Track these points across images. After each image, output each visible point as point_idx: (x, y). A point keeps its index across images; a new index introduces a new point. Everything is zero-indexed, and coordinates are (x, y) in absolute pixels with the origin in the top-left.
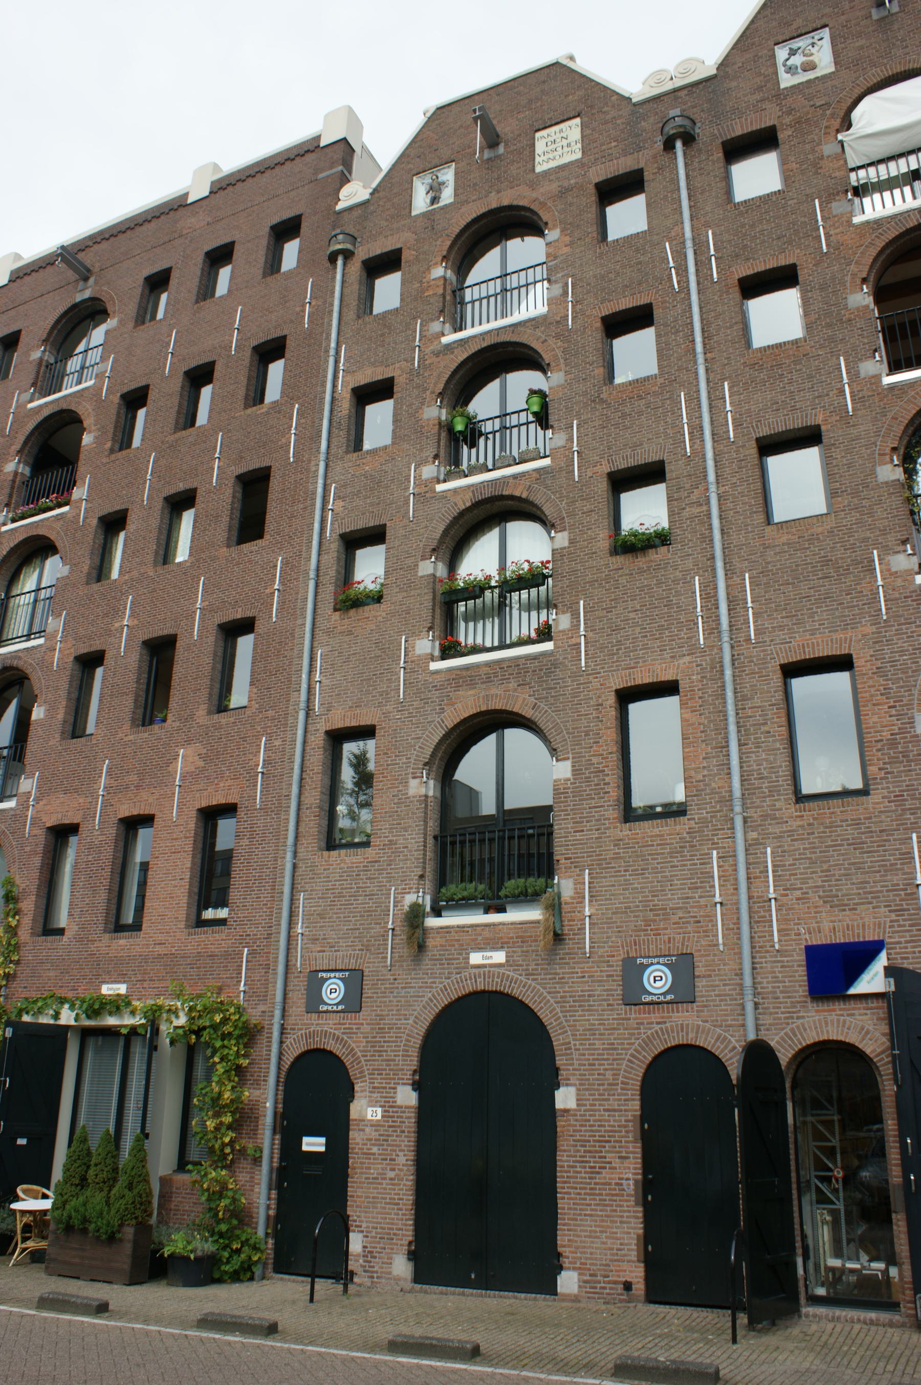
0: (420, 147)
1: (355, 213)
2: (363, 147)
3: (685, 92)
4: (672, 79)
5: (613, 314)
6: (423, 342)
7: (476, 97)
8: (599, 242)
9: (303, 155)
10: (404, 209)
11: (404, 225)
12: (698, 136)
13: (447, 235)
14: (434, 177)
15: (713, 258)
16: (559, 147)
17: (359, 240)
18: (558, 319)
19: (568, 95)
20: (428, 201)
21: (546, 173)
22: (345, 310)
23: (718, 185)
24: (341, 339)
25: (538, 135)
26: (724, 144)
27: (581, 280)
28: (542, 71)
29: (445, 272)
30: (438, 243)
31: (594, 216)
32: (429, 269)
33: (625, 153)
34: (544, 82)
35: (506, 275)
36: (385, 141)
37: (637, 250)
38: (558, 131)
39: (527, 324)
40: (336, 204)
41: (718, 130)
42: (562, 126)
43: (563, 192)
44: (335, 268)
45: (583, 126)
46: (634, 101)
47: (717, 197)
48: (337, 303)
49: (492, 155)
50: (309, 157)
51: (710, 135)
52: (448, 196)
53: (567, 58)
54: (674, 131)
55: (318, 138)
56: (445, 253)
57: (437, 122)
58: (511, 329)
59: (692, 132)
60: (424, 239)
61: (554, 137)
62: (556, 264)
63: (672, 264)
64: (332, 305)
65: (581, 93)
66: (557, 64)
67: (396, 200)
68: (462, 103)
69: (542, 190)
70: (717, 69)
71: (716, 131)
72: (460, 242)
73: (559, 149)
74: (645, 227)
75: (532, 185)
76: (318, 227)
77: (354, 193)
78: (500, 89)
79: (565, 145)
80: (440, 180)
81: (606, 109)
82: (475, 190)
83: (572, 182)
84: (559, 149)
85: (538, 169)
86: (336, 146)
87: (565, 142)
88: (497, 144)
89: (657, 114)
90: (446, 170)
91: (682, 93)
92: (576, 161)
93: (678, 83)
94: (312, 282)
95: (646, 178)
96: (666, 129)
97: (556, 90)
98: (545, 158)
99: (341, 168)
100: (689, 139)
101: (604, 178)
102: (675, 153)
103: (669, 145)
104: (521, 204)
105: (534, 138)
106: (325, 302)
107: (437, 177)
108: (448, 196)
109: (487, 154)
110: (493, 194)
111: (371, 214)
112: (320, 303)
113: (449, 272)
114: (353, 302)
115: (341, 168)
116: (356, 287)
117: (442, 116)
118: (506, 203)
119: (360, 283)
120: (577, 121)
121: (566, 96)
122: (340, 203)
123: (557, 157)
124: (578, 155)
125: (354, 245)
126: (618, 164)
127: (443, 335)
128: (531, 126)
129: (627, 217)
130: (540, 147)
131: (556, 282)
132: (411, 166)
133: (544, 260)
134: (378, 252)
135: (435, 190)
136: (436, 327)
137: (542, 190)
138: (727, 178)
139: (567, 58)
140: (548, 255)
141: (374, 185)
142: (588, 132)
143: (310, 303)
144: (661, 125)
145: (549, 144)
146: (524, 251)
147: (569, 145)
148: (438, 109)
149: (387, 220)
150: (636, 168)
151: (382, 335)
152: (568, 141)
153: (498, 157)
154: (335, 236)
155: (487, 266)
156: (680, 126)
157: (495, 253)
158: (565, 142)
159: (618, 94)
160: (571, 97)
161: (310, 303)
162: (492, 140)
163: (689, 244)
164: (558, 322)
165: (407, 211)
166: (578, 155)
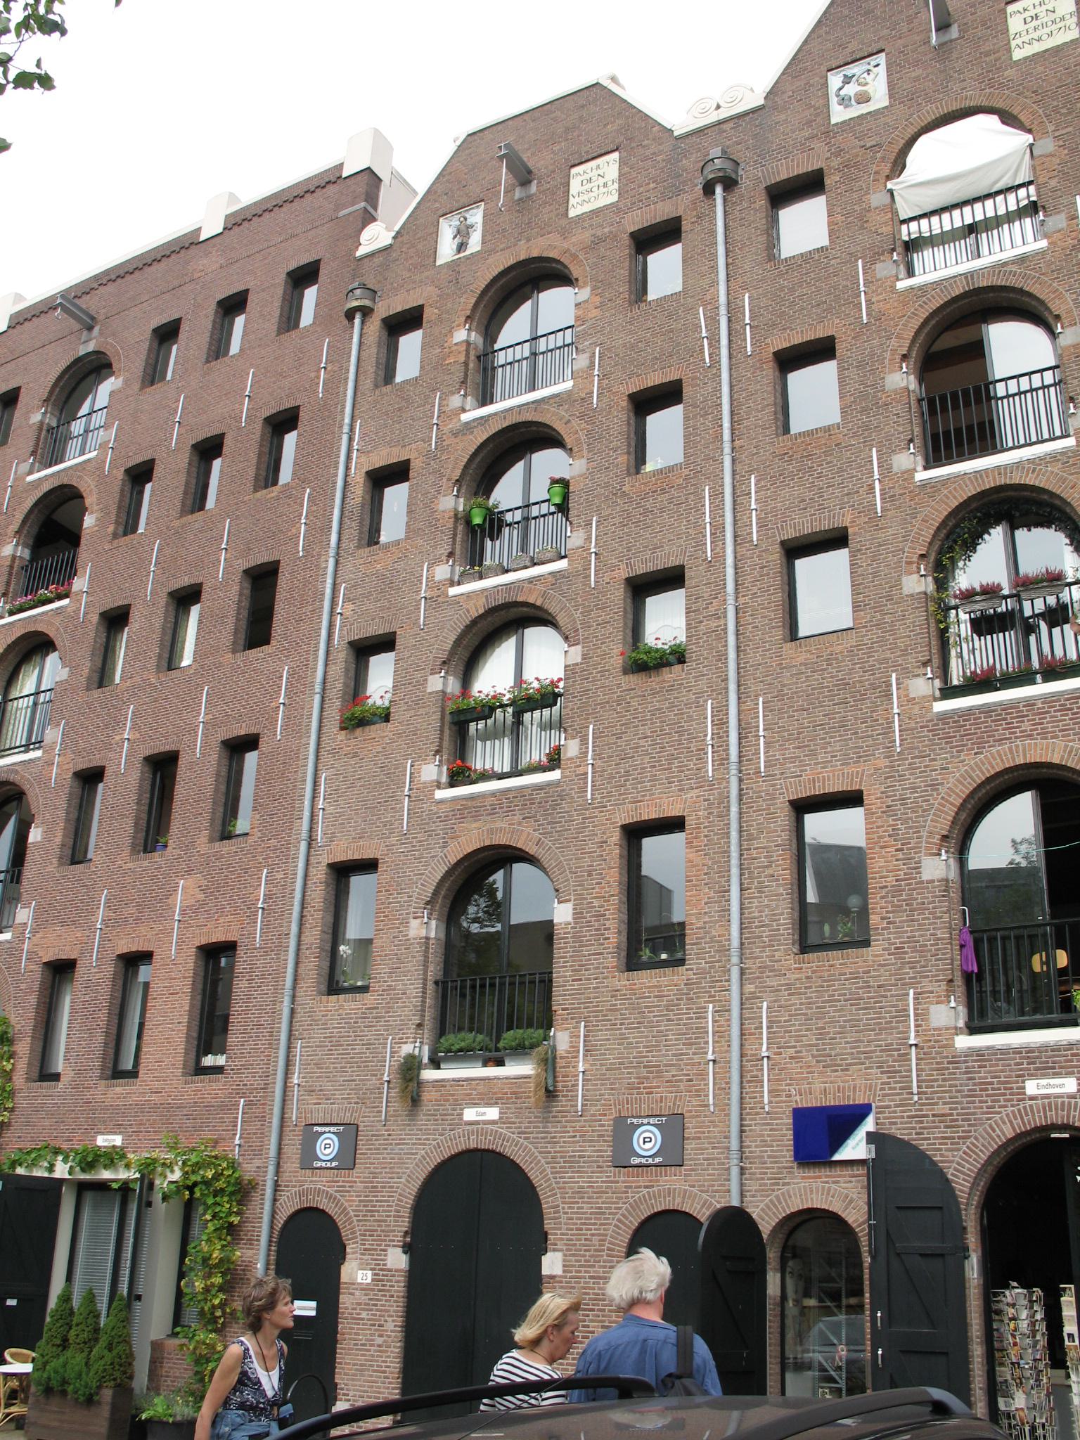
50: (331, 189)
87: (601, 181)
149: (410, 270)
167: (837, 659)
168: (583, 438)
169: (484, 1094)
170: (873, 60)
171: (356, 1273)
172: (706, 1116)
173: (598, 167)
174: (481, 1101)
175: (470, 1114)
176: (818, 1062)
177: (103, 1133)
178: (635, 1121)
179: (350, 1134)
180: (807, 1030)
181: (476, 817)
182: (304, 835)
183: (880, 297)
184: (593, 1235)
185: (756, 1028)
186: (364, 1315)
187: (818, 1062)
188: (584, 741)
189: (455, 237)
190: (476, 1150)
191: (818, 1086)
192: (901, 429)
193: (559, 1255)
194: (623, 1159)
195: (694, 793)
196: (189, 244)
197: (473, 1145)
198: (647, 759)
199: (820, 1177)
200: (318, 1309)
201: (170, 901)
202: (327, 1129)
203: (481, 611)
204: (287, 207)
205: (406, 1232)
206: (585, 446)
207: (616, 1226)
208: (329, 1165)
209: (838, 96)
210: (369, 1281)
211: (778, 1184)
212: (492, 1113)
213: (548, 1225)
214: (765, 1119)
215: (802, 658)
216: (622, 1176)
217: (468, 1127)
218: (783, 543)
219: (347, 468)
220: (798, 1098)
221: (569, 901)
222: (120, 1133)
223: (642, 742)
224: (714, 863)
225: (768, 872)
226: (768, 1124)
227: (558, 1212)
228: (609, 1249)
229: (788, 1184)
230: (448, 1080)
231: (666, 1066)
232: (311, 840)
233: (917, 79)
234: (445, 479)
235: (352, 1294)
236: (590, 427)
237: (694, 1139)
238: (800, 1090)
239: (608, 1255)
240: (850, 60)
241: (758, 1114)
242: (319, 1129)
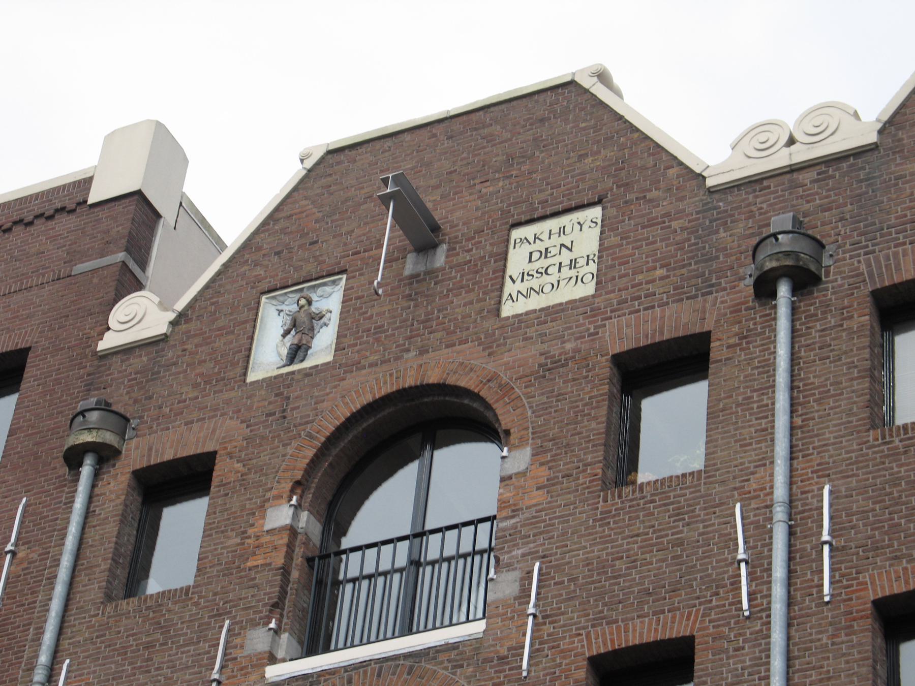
0: (284, 231)
1: (139, 361)
2: (185, 207)
3: (812, 174)
4: (791, 141)
5: (615, 652)
6: (227, 671)
7: (407, 137)
8: (605, 487)
9: (50, 218)
10: (234, 364)
11: (228, 402)
12: (827, 274)
13: (310, 435)
14: (303, 302)
15: (826, 548)
16: (553, 265)
17: (134, 423)
18: (504, 651)
19: (586, 155)
20: (285, 352)
21: (520, 319)
22: (82, 578)
23: (856, 385)
24: (65, 644)
25: (516, 234)
26: (875, 294)
27: (558, 568)
28: (542, 97)
29: (295, 516)
30: (290, 450)
31: (602, 427)
32: (262, 508)
33: (680, 295)
34: (542, 120)
35: (415, 536)
36: (233, 192)
37: (678, 514)
38: (555, 230)
39: (442, 657)
40: (101, 336)
41: (869, 265)
42: (565, 220)
43: (551, 366)
44: (76, 480)
45: (607, 227)
46: (710, 183)
47: (850, 413)
48: (66, 561)
49: (421, 268)
50: (64, 223)
51: (851, 276)
52: (323, 347)
53: (592, 75)
54: (774, 264)
55: (85, 183)
56: (299, 475)
57: (324, 181)
58: (408, 663)
59: (813, 268)
60: (263, 438)
61: (547, 243)
62: (514, 527)
63: (741, 555)
64: (57, 563)
65: (609, 153)
66: (571, 84)
67: (219, 344)
68: (378, 145)
69: (507, 358)
70: (880, 132)
71: (863, 267)
72: (335, 451)
73: (553, 270)
74: (698, 464)
75: (491, 345)
76: (57, 382)
77: (139, 318)
78: (457, 126)
79: (566, 262)
80: (313, 308)
81: (654, 194)
82: (378, 340)
83: (569, 346)
84: (553, 270)
85: (508, 310)
86: (119, 207)
87: (566, 257)
88: (435, 246)
89: (751, 215)
90: (328, 289)
91: (806, 177)
92: (582, 300)
93: (800, 154)
94: (26, 506)
95: (713, 355)
96: (760, 256)
97: (563, 140)
98: (523, 287)
99: (121, 256)
100: (805, 280)
101: (633, 345)
102: (775, 307)
103: (764, 289)
104: (462, 383)
105: (508, 241)
106: (44, 555)
107: (310, 302)
108: (323, 347)
109: (411, 265)
110: (412, 354)
111: (168, 366)
112: (35, 556)
113: (304, 516)
114: (101, 561)
115: (121, 256)
116: (112, 528)
117: (335, 170)
118: (433, 378)
119: (123, 520)
120: (596, 212)
121: (581, 157)
122: (107, 335)
123: (547, 288)
124: (588, 289)
125: (122, 435)
126: (663, 317)
127: (273, 659)
128: (505, 213)
129: (675, 428)
130: (517, 261)
131: (509, 567)
132: (260, 271)
133: (492, 511)
134: (169, 456)
135: (302, 329)
136: (258, 640)
137: (507, 358)
138: (882, 361)
139: (592, 75)
140: (503, 504)
141: (180, 305)
142: (614, 240)
143: (14, 553)
144: (758, 239)
145: (536, 256)
146: (465, 478)
147: (573, 264)
148: (330, 152)
149: (196, 386)
150: (697, 330)
151: (149, 646)
152: (572, 256)
153: (431, 273)
154: (82, 413)
155: (385, 510)
156: (787, 254)
157: (406, 477)
158: (566, 257)
159: (681, 164)
160: (590, 159)
161: (14, 553)
162: (423, 234)
163: (780, 513)
164: (501, 658)
165: (239, 370)
166: (588, 289)
173: (562, 231)
189: (286, 334)
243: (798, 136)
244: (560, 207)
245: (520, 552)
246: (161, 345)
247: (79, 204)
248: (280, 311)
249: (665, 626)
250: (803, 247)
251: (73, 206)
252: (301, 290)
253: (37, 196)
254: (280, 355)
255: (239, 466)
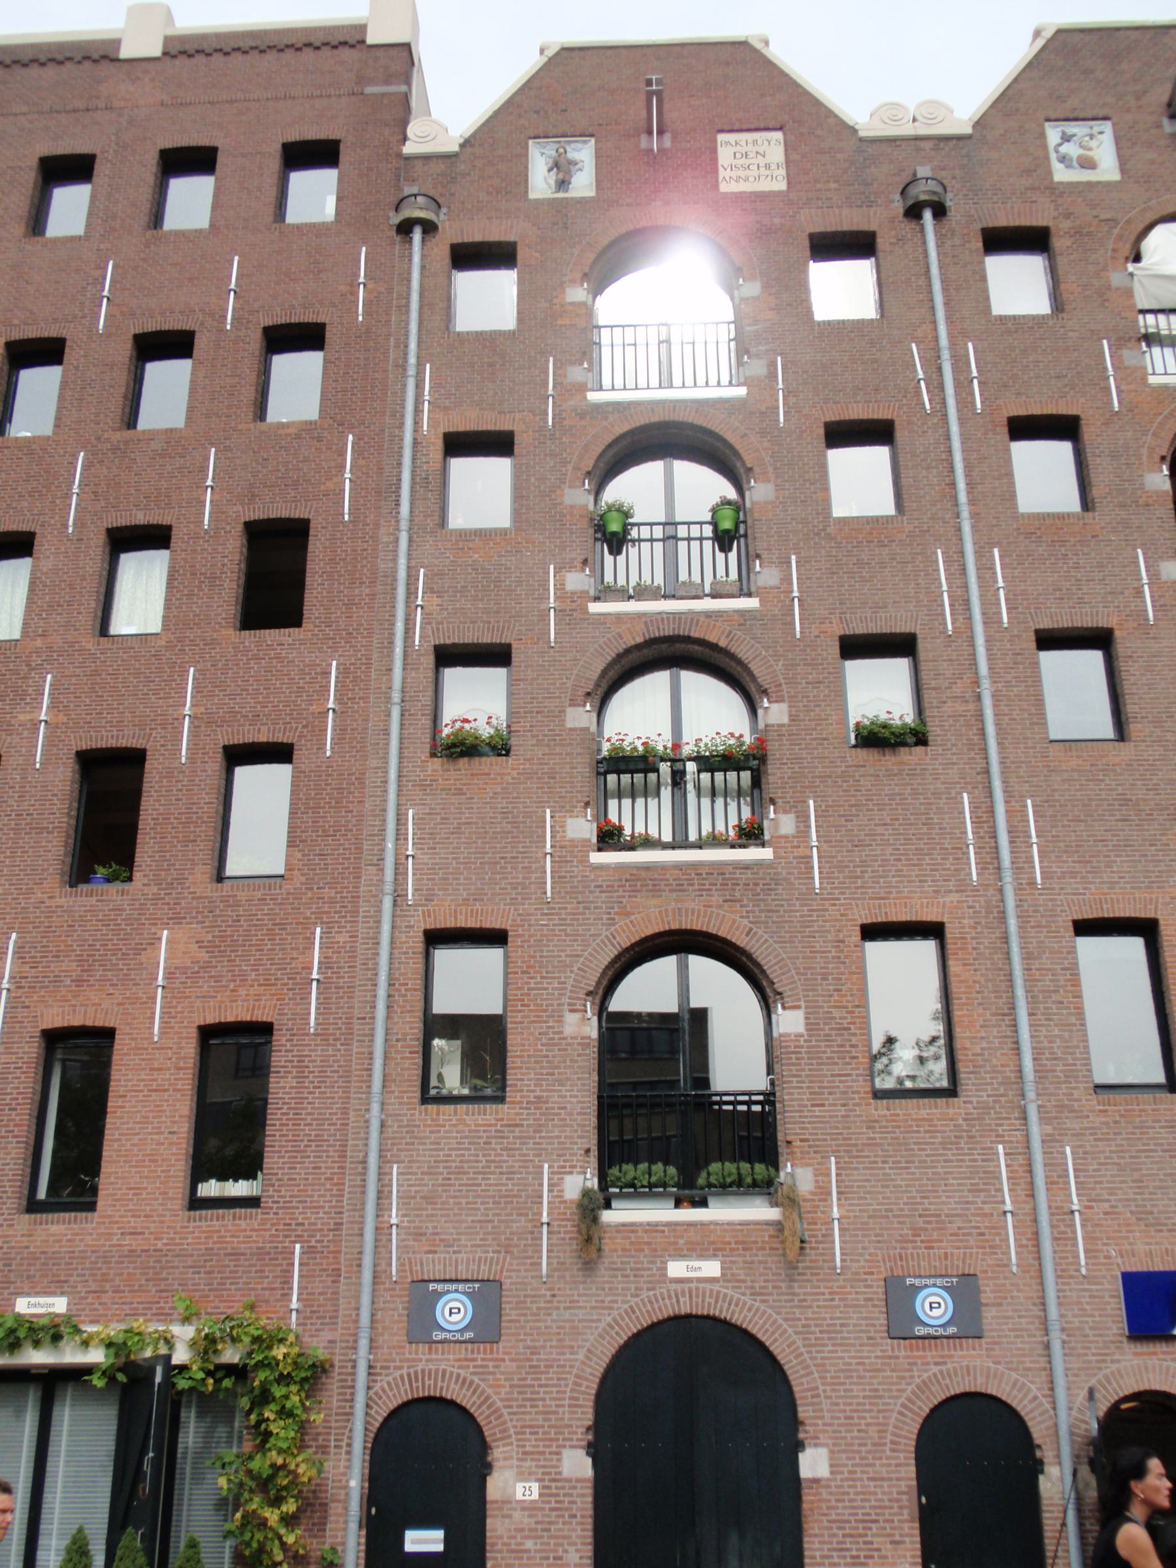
50: (345, 54)
83: (777, 221)
87: (761, 161)
90: (579, 145)
93: (923, 131)
98: (734, 174)
100: (940, 211)
121: (762, 96)
145: (738, 156)
149: (489, 193)
151: (491, 365)
167: (1114, 771)
168: (767, 459)
169: (701, 1242)
170: (1097, 126)
171: (512, 1487)
172: (1005, 1278)
173: (755, 142)
174: (691, 1252)
175: (677, 1269)
176: (1139, 1219)
177: (28, 1295)
178: (917, 1282)
179: (488, 1296)
180: (1122, 1182)
181: (656, 891)
182: (389, 887)
183: (1132, 387)
184: (868, 1425)
185: (1059, 1176)
186: (529, 1544)
187: (1139, 1219)
188: (803, 817)
189: (550, 170)
190: (689, 1316)
191: (1140, 1247)
192: (1167, 536)
193: (823, 1452)
194: (901, 1324)
195: (954, 897)
196: (97, 56)
197: (685, 1309)
198: (889, 850)
199: (1155, 1354)
200: (447, 1541)
201: (143, 958)
202: (454, 1286)
203: (639, 640)
204: (272, 56)
205: (588, 1429)
206: (770, 469)
207: (900, 1413)
208: (458, 1336)
209: (1057, 152)
210: (535, 1496)
211: (1105, 1361)
212: (711, 1268)
213: (803, 1412)
214: (1082, 1283)
215: (1073, 763)
216: (902, 1350)
217: (673, 1286)
218: (1037, 632)
219: (417, 423)
220: (1119, 1260)
221: (798, 1007)
222: (62, 1294)
223: (879, 830)
224: (987, 981)
225: (1055, 997)
226: (1085, 1290)
227: (818, 1396)
228: (892, 1442)
229: (1118, 1361)
230: (641, 1224)
231: (947, 1216)
232: (398, 897)
233: (1152, 162)
234: (570, 467)
235: (510, 1516)
236: (776, 449)
237: (993, 1305)
238: (1120, 1251)
239: (893, 1450)
240: (1071, 116)
241: (1071, 1277)
242: (440, 1287)
243: (918, 117)
244: (752, 126)
245: (764, 348)
246: (453, 159)
247: (359, 42)
248: (542, 154)
249: (873, 410)
250: (939, 189)
251: (211, 51)
252: (559, 142)
253: (343, 27)
254: (548, 184)
255: (537, 255)
